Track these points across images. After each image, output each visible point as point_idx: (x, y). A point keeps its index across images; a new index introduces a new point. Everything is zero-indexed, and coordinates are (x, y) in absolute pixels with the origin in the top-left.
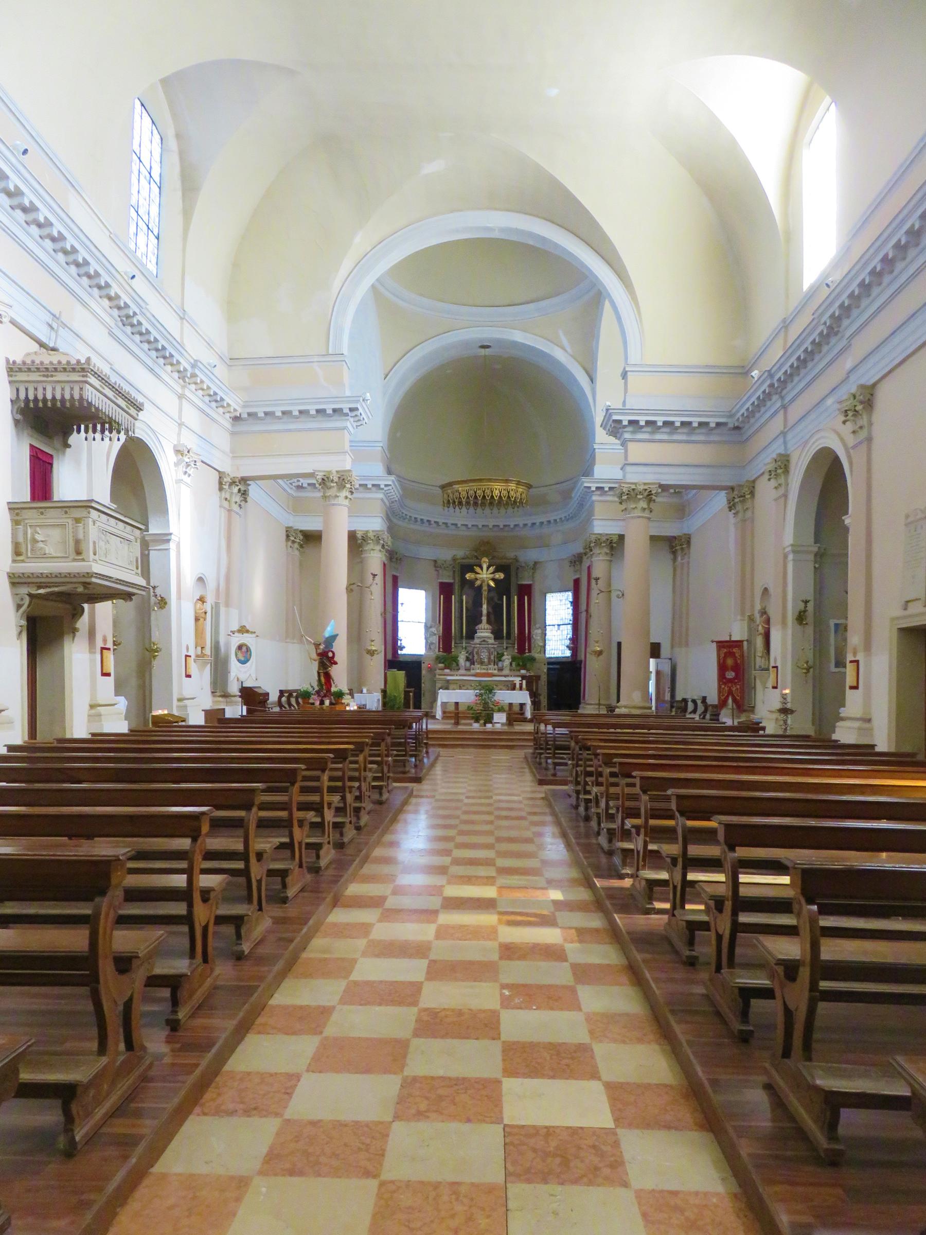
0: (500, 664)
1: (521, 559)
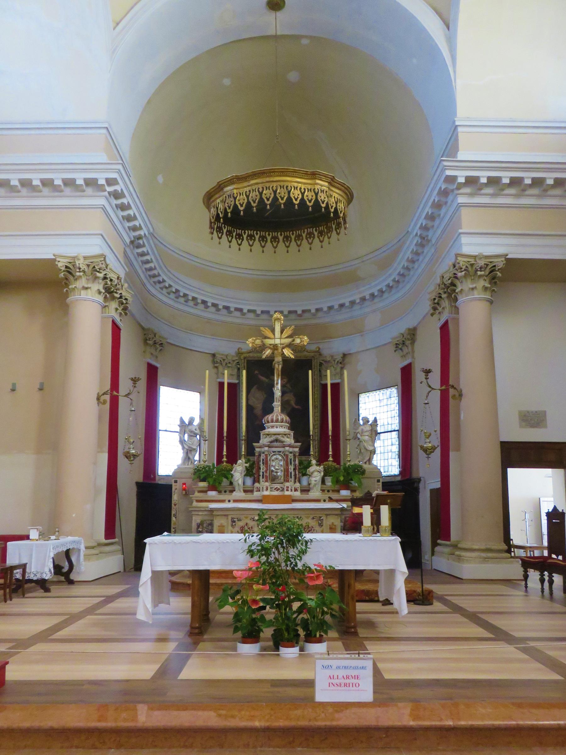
0: (304, 480)
1: (326, 352)
